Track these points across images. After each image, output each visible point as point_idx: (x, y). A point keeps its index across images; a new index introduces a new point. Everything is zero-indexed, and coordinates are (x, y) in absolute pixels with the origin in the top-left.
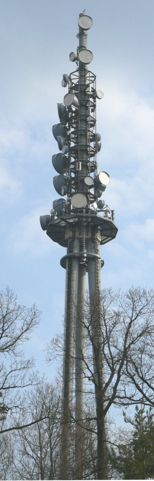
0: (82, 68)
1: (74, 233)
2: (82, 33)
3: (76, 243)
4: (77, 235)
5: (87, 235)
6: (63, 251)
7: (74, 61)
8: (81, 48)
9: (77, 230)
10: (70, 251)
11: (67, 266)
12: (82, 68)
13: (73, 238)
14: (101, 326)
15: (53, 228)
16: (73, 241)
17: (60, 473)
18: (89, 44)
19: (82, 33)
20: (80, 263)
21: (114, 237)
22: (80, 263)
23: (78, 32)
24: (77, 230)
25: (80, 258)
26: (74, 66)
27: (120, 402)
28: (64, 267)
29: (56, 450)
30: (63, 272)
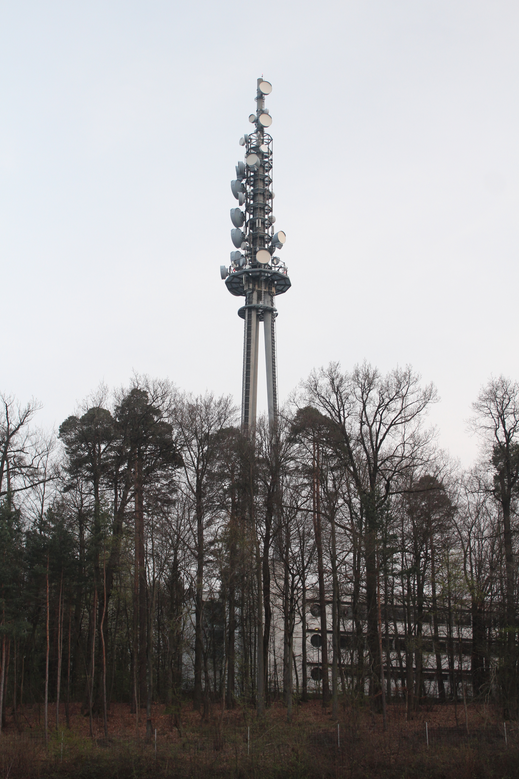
0: (260, 129)
1: (254, 285)
2: (260, 97)
3: (255, 295)
4: (257, 288)
5: (265, 289)
6: (241, 301)
7: (253, 123)
8: (261, 111)
9: (256, 283)
10: (248, 301)
11: (247, 315)
12: (260, 129)
13: (253, 290)
14: (265, 129)
15: (234, 284)
16: (252, 293)
17: (332, 449)
18: (267, 106)
19: (260, 97)
20: (258, 314)
21: (290, 285)
22: (258, 314)
23: (256, 95)
24: (256, 283)
25: (257, 309)
26: (253, 128)
27: (336, 388)
28: (244, 318)
29: (213, 528)
30: (241, 322)
